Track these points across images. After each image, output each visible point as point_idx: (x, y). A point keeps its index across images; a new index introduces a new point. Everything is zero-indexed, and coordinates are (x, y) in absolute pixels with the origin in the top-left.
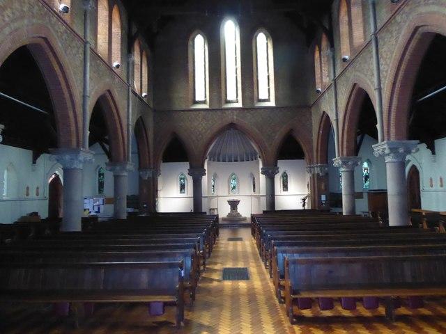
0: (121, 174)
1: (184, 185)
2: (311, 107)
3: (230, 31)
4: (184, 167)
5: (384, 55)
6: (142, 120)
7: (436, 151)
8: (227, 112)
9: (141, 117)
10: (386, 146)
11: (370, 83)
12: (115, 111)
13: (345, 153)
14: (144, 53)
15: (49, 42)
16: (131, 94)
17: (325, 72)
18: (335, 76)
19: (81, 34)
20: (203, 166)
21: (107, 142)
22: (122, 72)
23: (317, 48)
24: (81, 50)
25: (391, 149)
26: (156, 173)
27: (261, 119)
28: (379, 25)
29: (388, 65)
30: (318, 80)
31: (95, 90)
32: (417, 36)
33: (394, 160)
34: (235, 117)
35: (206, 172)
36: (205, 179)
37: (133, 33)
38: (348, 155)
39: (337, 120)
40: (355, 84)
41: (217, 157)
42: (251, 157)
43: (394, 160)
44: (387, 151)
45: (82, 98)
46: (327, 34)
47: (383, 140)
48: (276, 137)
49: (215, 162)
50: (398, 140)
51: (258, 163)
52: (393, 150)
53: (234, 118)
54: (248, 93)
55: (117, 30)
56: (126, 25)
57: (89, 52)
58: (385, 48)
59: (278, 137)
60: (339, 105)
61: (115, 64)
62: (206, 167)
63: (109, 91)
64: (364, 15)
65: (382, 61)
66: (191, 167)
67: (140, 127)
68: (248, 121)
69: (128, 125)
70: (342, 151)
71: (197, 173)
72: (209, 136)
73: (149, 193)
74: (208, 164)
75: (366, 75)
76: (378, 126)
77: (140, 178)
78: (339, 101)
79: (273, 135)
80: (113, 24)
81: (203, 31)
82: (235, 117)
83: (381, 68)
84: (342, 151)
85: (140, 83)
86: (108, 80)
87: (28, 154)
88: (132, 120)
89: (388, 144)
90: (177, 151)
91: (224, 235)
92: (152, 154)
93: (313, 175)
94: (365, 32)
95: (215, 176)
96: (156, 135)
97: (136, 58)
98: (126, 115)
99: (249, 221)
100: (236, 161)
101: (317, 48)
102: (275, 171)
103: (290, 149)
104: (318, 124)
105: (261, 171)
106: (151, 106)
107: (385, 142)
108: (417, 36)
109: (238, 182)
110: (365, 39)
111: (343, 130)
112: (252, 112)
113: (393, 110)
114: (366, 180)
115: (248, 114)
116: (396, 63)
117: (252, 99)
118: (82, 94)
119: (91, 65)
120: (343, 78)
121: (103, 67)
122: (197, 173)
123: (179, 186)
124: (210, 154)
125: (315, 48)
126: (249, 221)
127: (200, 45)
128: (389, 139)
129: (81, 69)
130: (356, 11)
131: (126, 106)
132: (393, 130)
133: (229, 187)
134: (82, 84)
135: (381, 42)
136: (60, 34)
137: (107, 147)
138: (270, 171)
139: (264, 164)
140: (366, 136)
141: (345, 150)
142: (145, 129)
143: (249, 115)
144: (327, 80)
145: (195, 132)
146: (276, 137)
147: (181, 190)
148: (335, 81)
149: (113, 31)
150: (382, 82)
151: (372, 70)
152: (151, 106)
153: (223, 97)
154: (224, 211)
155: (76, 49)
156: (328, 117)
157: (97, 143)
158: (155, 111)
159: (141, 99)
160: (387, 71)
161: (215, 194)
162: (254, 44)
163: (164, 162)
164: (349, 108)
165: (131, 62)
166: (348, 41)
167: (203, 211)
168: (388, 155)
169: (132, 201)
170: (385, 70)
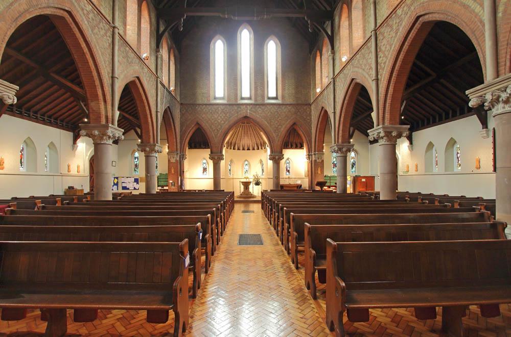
1: (206, 169)
2: (311, 105)
3: (245, 37)
4: (206, 153)
5: (383, 49)
6: (170, 109)
7: (413, 142)
8: (242, 107)
9: (168, 107)
10: (381, 130)
11: (367, 76)
13: (340, 141)
14: (172, 51)
16: (159, 85)
17: (325, 73)
18: (334, 75)
19: (110, 18)
20: (221, 152)
21: (140, 127)
22: (152, 65)
23: (318, 54)
24: (109, 34)
25: (385, 132)
26: (183, 157)
27: (270, 114)
28: (379, 22)
29: (387, 57)
30: (318, 82)
31: (124, 74)
32: (418, 25)
33: (387, 143)
34: (249, 111)
35: (224, 157)
36: (223, 163)
37: (160, 32)
38: (342, 143)
39: (335, 113)
40: (353, 79)
41: (232, 146)
43: (387, 143)
44: (382, 134)
45: (111, 79)
46: (329, 39)
48: (282, 129)
49: (232, 150)
51: (266, 151)
52: (388, 134)
53: (248, 112)
54: (259, 92)
55: (146, 26)
56: (154, 20)
57: (117, 37)
58: (385, 42)
59: (283, 129)
60: (337, 100)
61: (145, 55)
62: (224, 153)
63: (138, 78)
64: (364, 15)
65: (380, 54)
66: (212, 152)
67: (168, 115)
68: (258, 115)
69: (157, 112)
71: (216, 158)
72: (227, 127)
73: (178, 170)
75: (364, 70)
77: (169, 161)
80: (142, 20)
81: (225, 39)
82: (249, 111)
83: (379, 60)
85: (168, 75)
86: (137, 67)
87: (69, 135)
88: (161, 109)
89: (383, 128)
90: (199, 140)
91: (238, 208)
93: (312, 161)
94: (364, 27)
95: (231, 161)
97: (164, 52)
98: (154, 102)
100: (249, 149)
101: (318, 54)
102: (281, 157)
103: (292, 140)
104: (317, 119)
106: (179, 100)
107: (381, 126)
108: (418, 25)
109: (250, 167)
110: (364, 37)
111: (340, 121)
112: (263, 107)
113: (388, 98)
114: (353, 167)
115: (260, 109)
116: (395, 53)
117: (263, 97)
118: (111, 75)
119: (119, 49)
120: (341, 75)
121: (132, 55)
122: (216, 158)
123: (202, 169)
125: (316, 54)
127: (219, 48)
128: (383, 123)
129: (110, 51)
130: (357, 14)
131: (155, 94)
132: (387, 116)
133: (242, 171)
134: (111, 66)
135: (380, 37)
136: (85, 12)
139: (272, 151)
140: (306, 184)
142: (172, 118)
143: (260, 110)
144: (326, 81)
145: (212, 123)
146: (282, 129)
147: (204, 172)
148: (334, 79)
149: (142, 25)
150: (379, 73)
151: (370, 65)
152: (179, 100)
154: (239, 190)
155: (104, 31)
156: (326, 112)
158: (181, 104)
159: (169, 92)
160: (385, 63)
161: (231, 177)
162: (265, 50)
165: (159, 56)
166: (348, 43)
167: (222, 189)
168: (382, 138)
169: (162, 178)
170: (383, 62)
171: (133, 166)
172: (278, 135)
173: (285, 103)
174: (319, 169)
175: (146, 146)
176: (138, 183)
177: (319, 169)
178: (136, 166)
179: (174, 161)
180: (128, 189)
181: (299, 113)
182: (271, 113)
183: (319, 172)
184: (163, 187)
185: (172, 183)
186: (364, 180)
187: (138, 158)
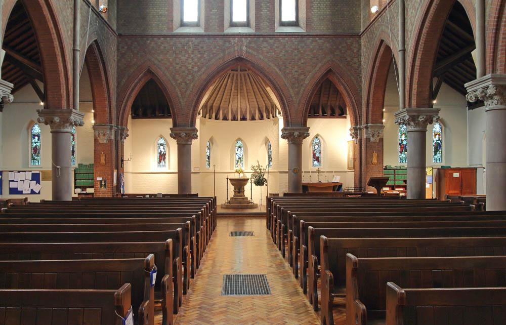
0: (62, 130)
1: (164, 155)
4: (165, 126)
9: (96, 41)
10: (490, 83)
12: (51, 25)
13: (414, 102)
15: (50, 5)
20: (193, 123)
21: (43, 79)
25: (497, 86)
26: (121, 134)
34: (244, 48)
35: (198, 134)
36: (195, 144)
38: (418, 106)
39: (404, 51)
41: (213, 112)
42: (266, 112)
44: (491, 91)
47: (484, 74)
48: (306, 82)
50: (284, 288)
51: (276, 122)
53: (244, 49)
59: (309, 82)
60: (409, 26)
66: (175, 125)
67: (94, 57)
68: (263, 56)
69: (74, 50)
70: (410, 98)
72: (204, 77)
74: (201, 122)
76: (476, 54)
78: (408, 21)
79: (302, 77)
82: (244, 48)
84: (410, 98)
89: (493, 78)
91: (224, 228)
92: (114, 103)
93: (361, 140)
96: (121, 74)
99: (263, 210)
105: (281, 133)
107: (489, 76)
109: (246, 151)
112: (271, 41)
115: (265, 44)
124: (205, 106)
126: (263, 210)
128: (494, 70)
131: (71, 18)
137: (41, 86)
138: (296, 133)
139: (287, 122)
141: (414, 98)
146: (306, 82)
147: (160, 162)
153: (227, 17)
156: (388, 49)
157: (266, 212)
158: (120, 35)
159: (98, 14)
163: (136, 116)
164: (425, 31)
167: (193, 193)
168: (491, 97)
171: (30, 152)
172: (298, 93)
173: (313, 32)
174: (375, 155)
175: (54, 114)
176: (38, 182)
177: (375, 155)
178: (36, 150)
179: (105, 141)
180: (21, 193)
181: (337, 53)
182: (286, 51)
183: (375, 160)
184: (84, 188)
185: (101, 181)
186: (456, 175)
187: (38, 136)
